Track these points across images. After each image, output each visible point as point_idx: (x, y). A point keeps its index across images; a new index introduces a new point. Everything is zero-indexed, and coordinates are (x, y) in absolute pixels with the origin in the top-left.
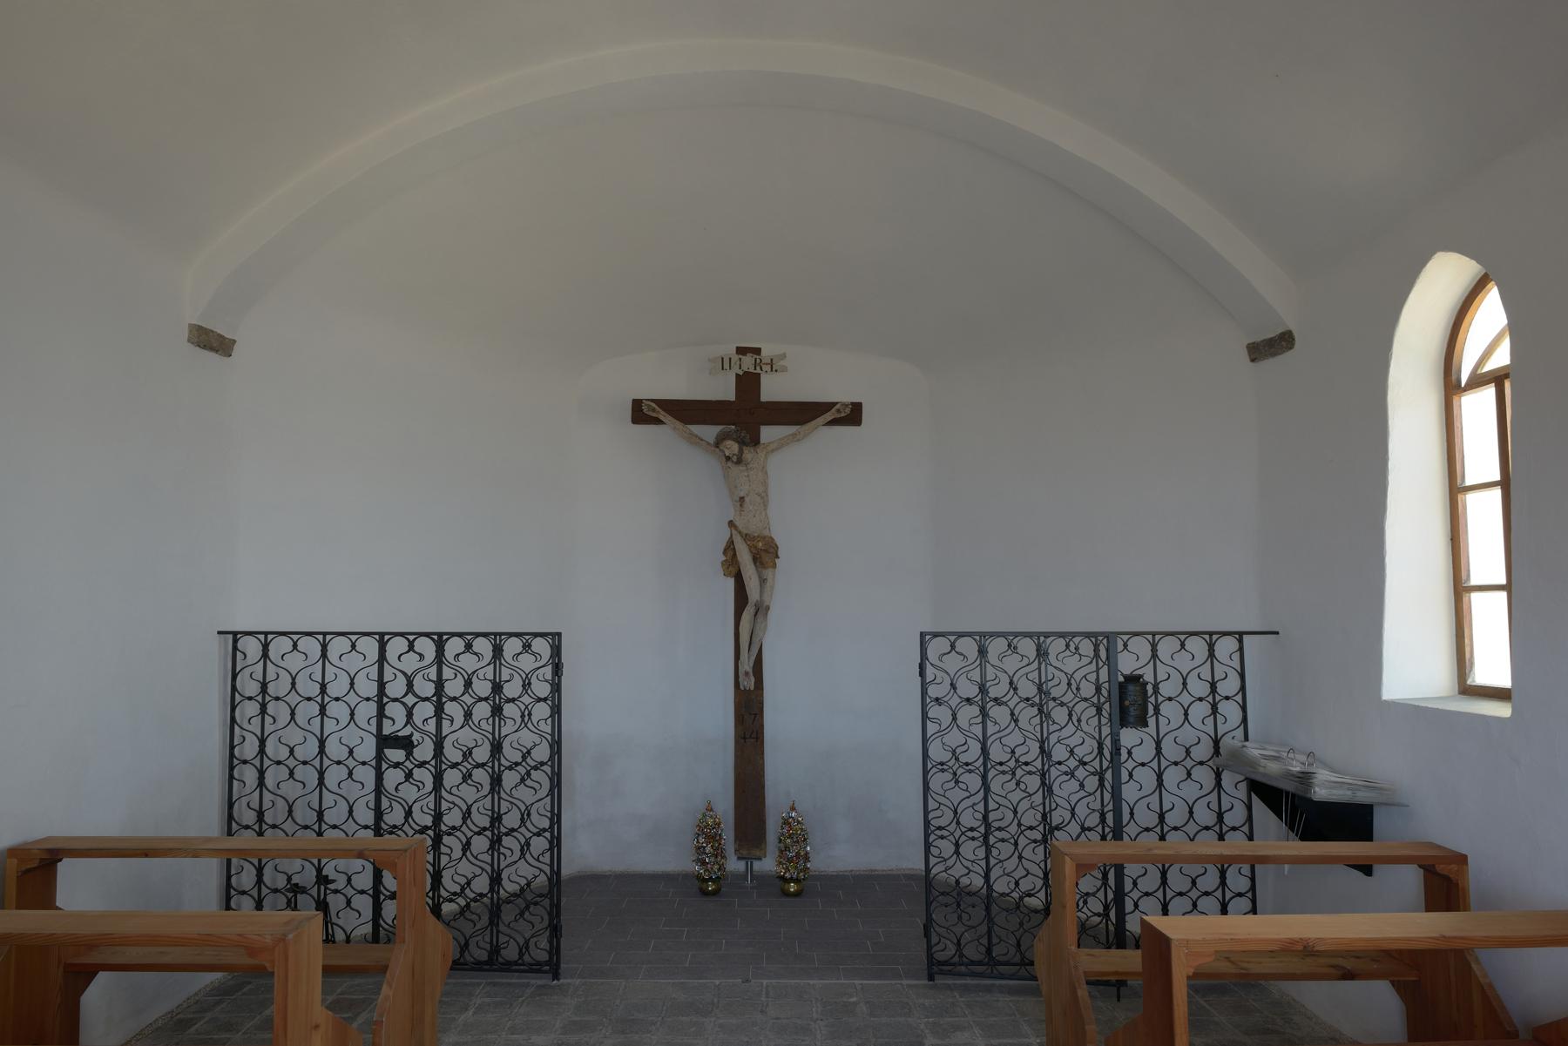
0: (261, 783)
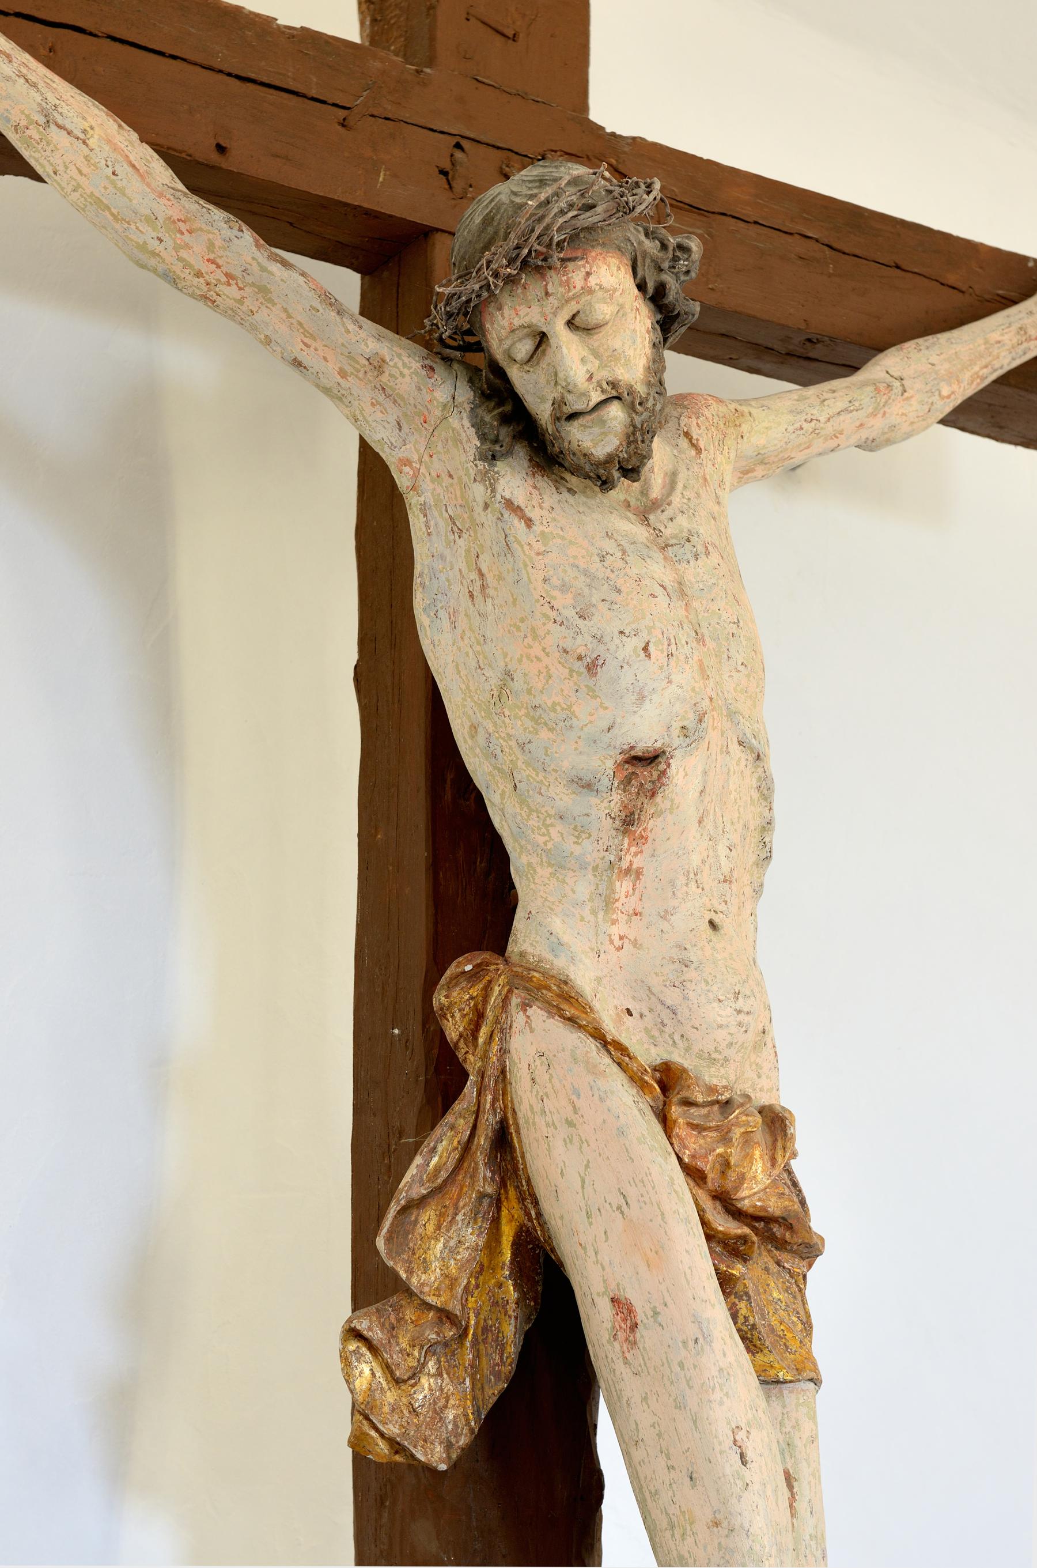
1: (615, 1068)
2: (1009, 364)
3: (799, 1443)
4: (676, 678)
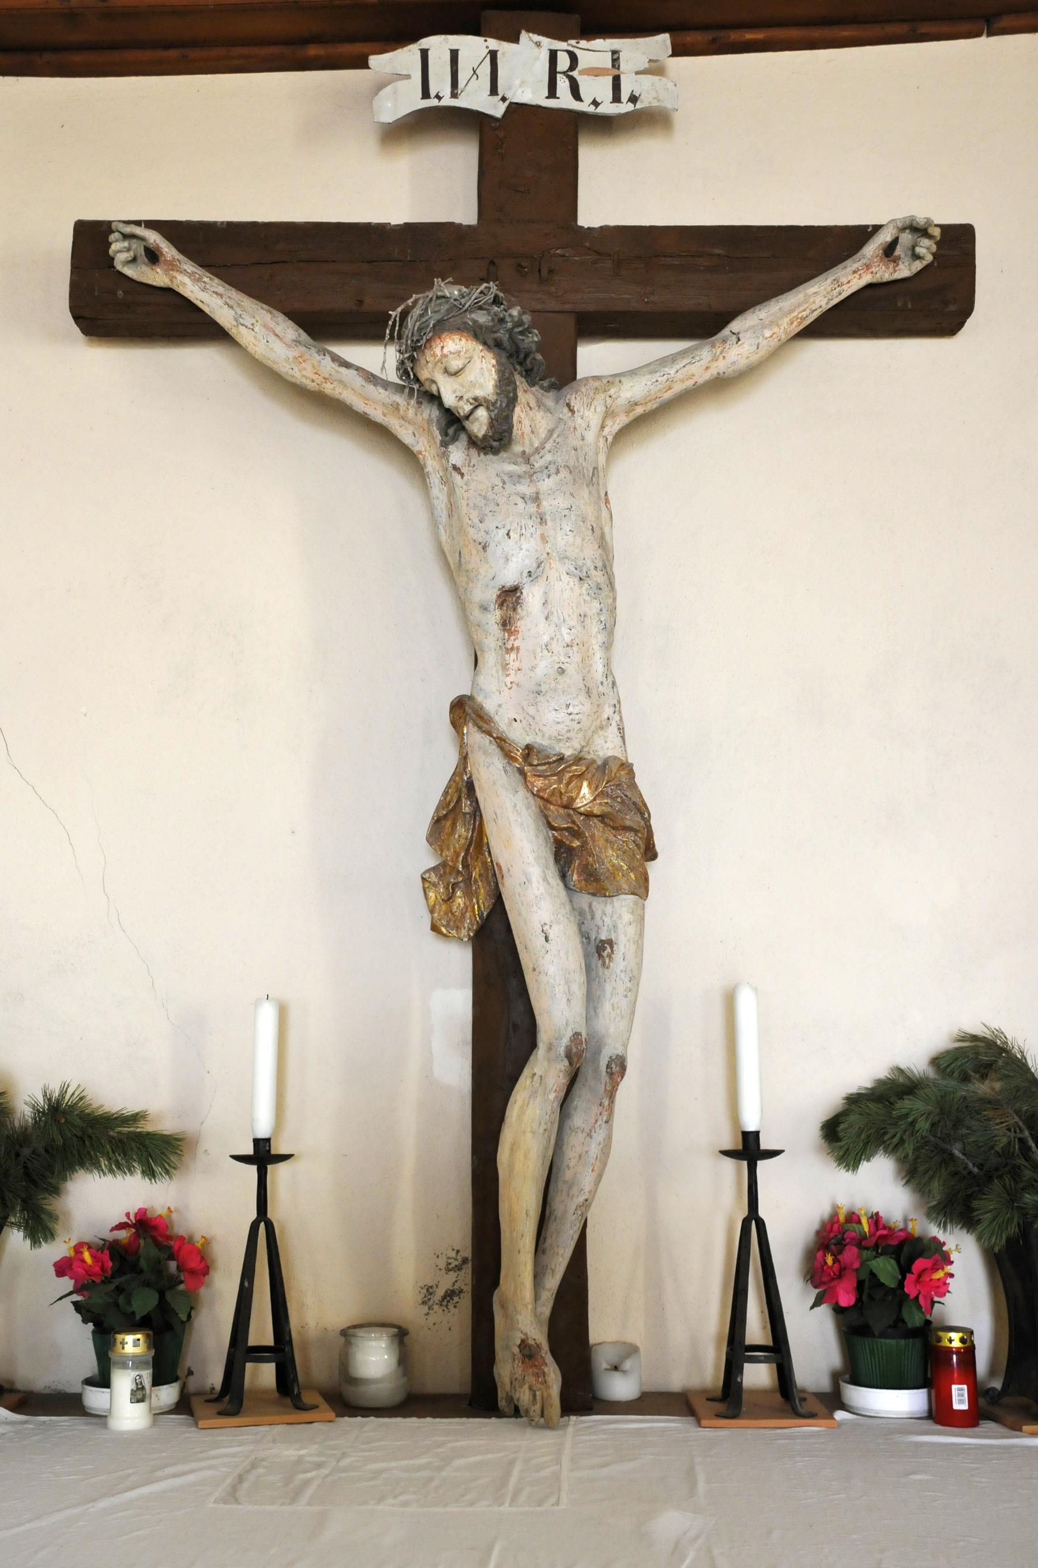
1: (497, 750)
2: (827, 303)
3: (620, 926)
4: (525, 546)
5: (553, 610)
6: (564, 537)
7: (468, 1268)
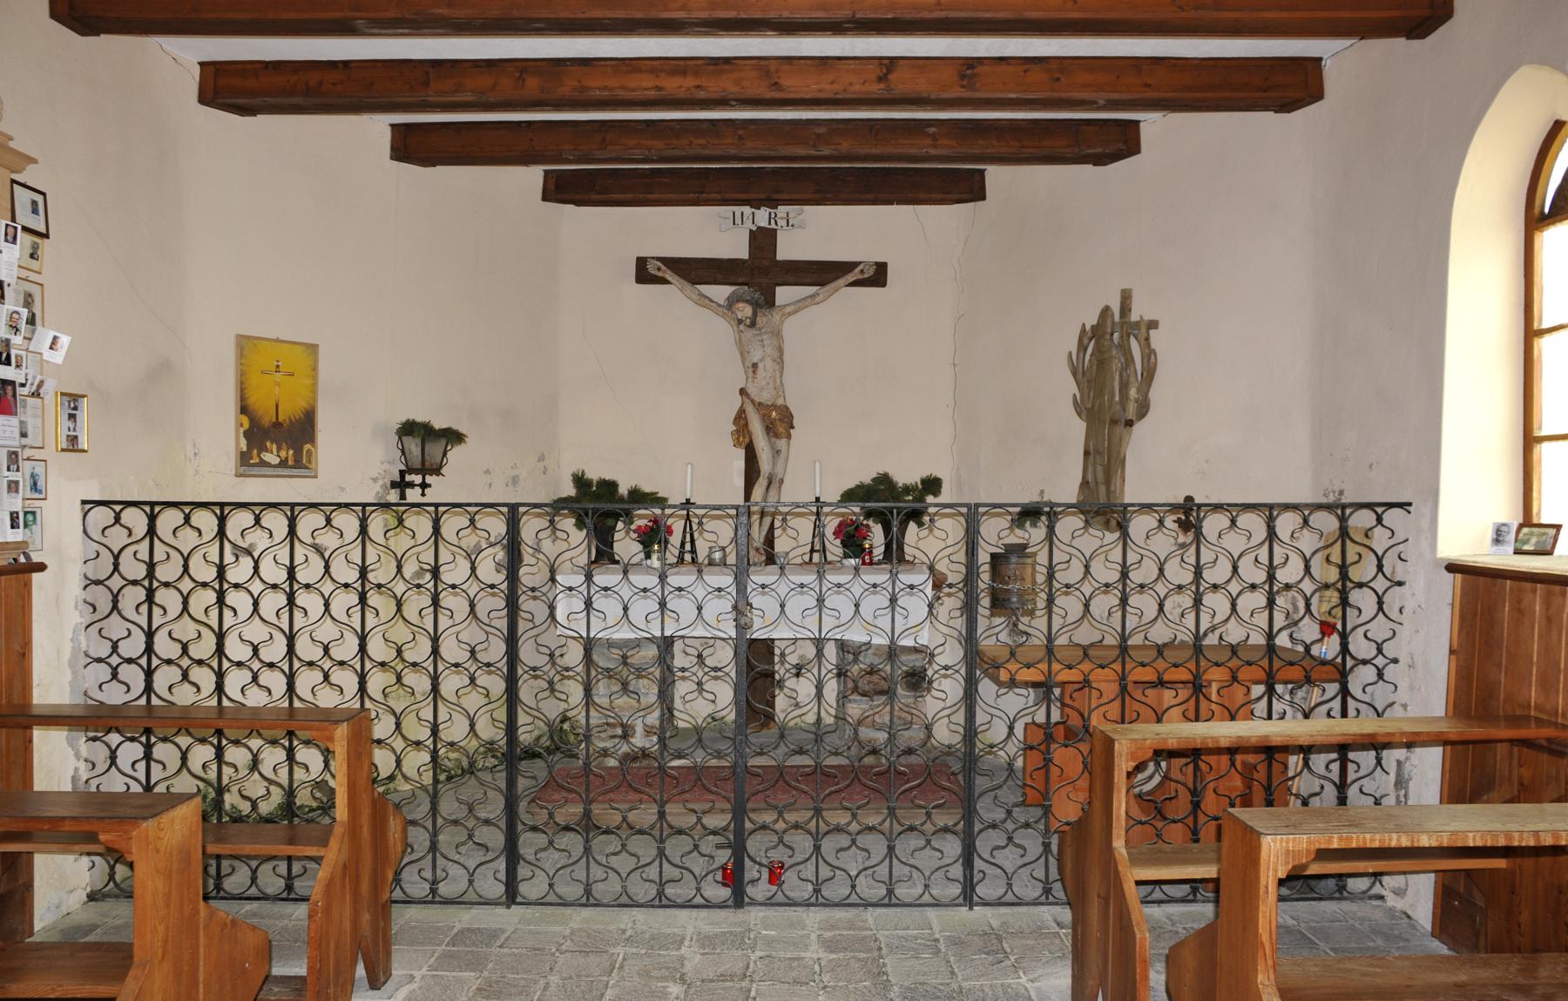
0: (363, 639)
5: (767, 369)
6: (769, 350)
7: (746, 880)
